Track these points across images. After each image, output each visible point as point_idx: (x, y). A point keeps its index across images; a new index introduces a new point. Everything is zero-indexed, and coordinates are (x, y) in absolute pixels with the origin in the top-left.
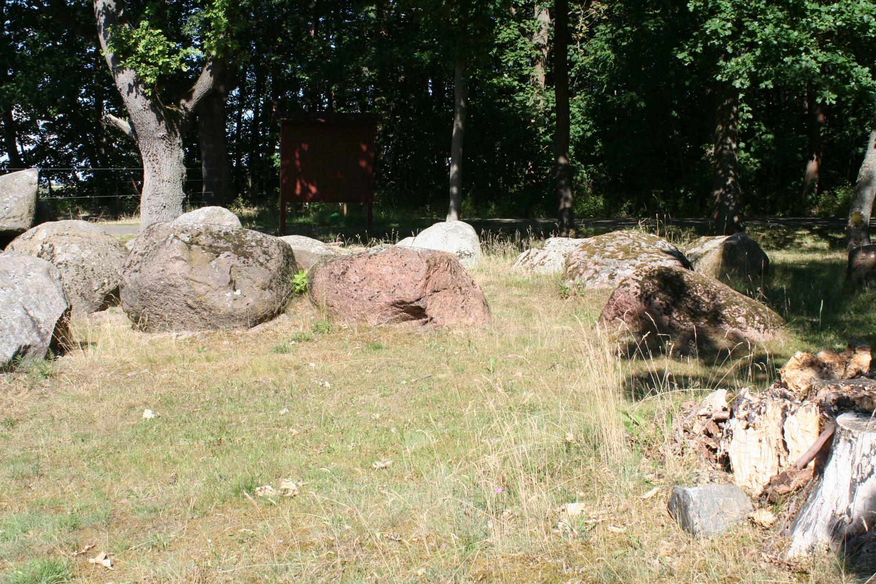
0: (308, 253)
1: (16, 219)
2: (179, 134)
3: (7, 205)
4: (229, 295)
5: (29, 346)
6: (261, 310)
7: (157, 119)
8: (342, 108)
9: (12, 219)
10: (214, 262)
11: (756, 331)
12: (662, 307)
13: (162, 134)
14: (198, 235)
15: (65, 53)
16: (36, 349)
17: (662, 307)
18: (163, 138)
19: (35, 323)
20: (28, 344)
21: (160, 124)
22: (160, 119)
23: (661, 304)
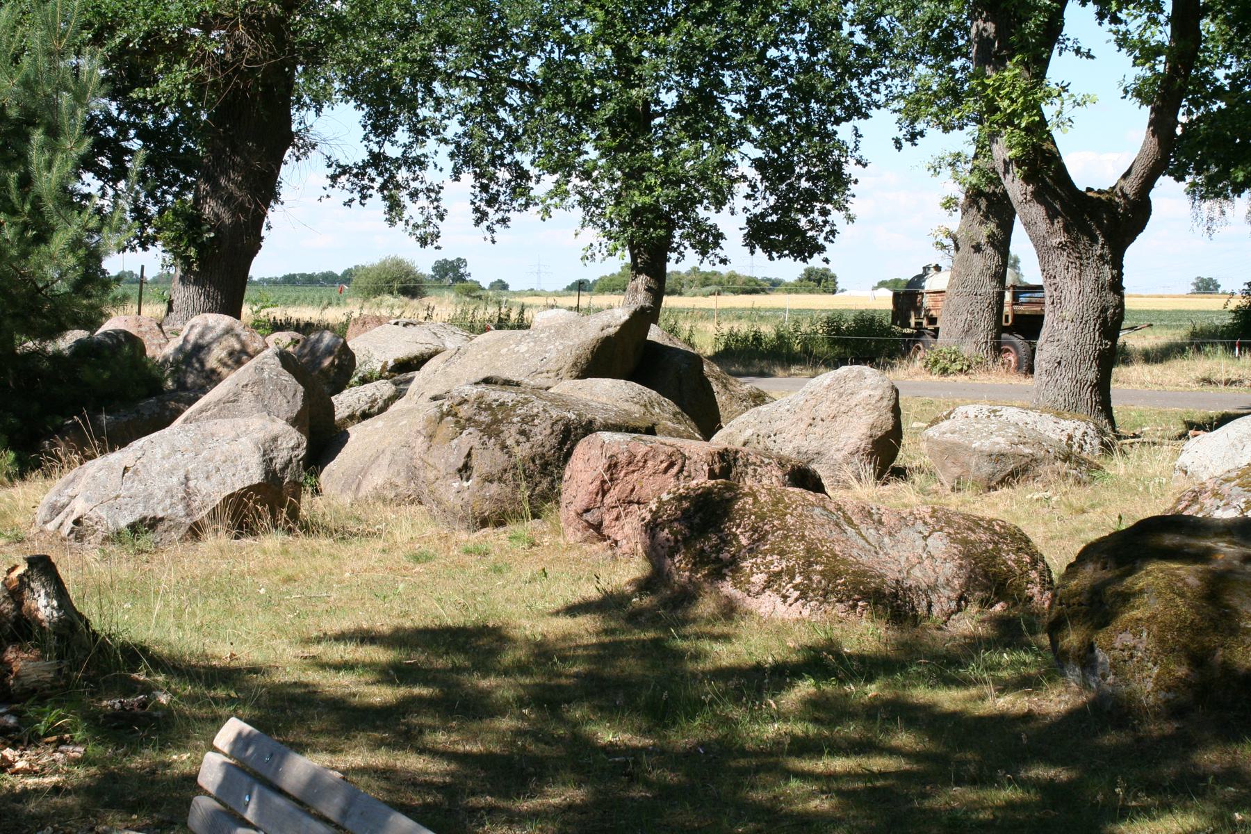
0: (967, 449)
1: (550, 375)
2: (1101, 240)
3: (547, 355)
4: (456, 485)
5: (162, 519)
6: (488, 508)
7: (1047, 214)
8: (1117, 199)
9: (545, 374)
10: (456, 441)
11: (779, 600)
12: (668, 544)
13: (1058, 240)
14: (460, 404)
15: (184, 202)
16: (172, 523)
17: (668, 544)
18: (1062, 247)
19: (188, 496)
20: (160, 515)
21: (1053, 224)
22: (1052, 215)
23: (668, 540)
